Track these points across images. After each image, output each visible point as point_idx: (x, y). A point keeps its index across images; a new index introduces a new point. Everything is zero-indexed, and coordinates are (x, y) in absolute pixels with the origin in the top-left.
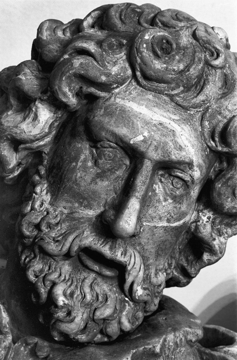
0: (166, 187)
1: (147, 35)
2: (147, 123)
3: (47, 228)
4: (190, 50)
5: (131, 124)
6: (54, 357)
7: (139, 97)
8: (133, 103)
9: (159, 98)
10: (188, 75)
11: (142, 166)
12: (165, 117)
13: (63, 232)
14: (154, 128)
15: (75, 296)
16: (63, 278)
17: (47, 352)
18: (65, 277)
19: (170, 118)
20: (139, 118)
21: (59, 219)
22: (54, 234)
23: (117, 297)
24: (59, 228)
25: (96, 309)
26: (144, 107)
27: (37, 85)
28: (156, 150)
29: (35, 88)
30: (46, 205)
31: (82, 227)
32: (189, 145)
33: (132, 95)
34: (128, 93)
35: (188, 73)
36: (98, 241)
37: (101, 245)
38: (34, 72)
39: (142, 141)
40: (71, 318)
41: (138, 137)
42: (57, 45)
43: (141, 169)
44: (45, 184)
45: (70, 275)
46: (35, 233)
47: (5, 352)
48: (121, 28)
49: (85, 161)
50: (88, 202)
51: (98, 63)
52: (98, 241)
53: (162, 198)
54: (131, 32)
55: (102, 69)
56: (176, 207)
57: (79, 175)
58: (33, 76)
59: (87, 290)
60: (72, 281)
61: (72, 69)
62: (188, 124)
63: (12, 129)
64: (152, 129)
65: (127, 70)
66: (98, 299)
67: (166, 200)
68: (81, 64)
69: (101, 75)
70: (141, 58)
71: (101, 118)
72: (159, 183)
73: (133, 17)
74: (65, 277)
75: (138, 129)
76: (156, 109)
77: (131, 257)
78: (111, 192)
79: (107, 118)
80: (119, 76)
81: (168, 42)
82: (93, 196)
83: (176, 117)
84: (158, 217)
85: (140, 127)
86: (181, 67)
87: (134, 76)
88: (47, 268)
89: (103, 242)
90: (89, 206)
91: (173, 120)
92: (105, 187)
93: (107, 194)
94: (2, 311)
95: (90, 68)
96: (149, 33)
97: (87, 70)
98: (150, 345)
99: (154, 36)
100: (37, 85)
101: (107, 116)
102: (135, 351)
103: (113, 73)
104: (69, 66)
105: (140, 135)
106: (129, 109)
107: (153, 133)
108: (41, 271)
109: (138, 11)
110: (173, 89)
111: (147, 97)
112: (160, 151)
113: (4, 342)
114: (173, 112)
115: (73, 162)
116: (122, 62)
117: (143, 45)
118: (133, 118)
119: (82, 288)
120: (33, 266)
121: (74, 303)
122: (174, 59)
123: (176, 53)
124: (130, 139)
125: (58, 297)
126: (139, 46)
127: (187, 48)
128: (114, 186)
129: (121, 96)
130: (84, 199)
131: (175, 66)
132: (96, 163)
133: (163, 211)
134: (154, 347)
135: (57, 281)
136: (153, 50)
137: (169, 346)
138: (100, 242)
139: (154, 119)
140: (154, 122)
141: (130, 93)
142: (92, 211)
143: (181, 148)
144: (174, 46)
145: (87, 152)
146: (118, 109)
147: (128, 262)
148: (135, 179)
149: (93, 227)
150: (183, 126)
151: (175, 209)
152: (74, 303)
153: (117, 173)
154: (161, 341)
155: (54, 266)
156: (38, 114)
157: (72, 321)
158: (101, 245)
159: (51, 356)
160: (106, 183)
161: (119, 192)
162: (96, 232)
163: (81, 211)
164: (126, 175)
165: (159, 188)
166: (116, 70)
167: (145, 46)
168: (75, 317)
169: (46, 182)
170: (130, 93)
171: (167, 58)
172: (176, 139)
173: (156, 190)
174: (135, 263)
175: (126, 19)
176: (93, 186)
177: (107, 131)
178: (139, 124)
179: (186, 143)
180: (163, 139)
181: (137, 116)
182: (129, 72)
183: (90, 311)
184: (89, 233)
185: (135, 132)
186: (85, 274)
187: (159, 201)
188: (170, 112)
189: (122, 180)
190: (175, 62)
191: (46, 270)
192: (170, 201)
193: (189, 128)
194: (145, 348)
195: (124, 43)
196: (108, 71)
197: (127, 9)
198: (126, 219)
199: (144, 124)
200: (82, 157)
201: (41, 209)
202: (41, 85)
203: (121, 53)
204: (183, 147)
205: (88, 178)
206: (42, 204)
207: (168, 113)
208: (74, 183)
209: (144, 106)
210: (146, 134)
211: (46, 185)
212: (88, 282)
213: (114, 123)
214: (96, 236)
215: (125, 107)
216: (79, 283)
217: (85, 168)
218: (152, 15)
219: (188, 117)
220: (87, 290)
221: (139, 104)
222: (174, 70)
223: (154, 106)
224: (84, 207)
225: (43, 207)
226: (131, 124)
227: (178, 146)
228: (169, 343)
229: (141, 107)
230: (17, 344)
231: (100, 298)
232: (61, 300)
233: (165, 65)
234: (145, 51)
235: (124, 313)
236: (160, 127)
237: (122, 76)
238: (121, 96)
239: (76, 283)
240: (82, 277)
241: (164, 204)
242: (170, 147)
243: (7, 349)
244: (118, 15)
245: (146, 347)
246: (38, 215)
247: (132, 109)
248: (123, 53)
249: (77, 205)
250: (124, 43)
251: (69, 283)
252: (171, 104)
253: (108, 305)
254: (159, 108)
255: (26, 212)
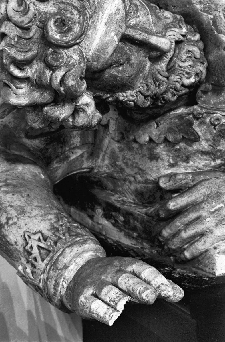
0: (133, 17)
1: (56, 37)
2: (106, 34)
3: (149, 91)
4: (61, 6)
5: (107, 44)
6: (214, 80)
7: (90, 39)
8: (93, 43)
9: (91, 26)
10: (80, 7)
11: (129, 35)
12: (101, 21)
13: (153, 81)
14: (109, 28)
15: (189, 71)
16: (179, 80)
17: (209, 85)
18: (179, 78)
19: (102, 18)
20: (103, 39)
21: (145, 85)
22: (153, 87)
23: (187, 45)
24: (150, 84)
25: (195, 58)
26: (96, 36)
27: (69, 106)
28: (121, 26)
29: (71, 107)
30: (133, 93)
31: (154, 70)
32: (114, 3)
33: (89, 44)
34: (86, 47)
35: (78, 7)
36: (164, 60)
37: (167, 58)
38: (59, 108)
39: (117, 36)
40: (200, 73)
41: (115, 40)
42: (35, 93)
43: (131, 36)
44: (119, 94)
45: (177, 75)
46: (149, 98)
47: (204, 109)
48: (35, 52)
49: (118, 71)
50: (142, 67)
51: (73, 69)
52: (164, 60)
53: (138, 19)
54: (39, 45)
55: (76, 66)
56: (141, 9)
57: (126, 75)
58: (62, 108)
59: (186, 64)
60: (181, 74)
61: (76, 85)
62: (103, 5)
63: (89, 119)
64: (110, 30)
65: (75, 49)
66: (190, 57)
67: (139, 17)
68: (73, 80)
69: (81, 67)
70: (72, 40)
71: (99, 64)
72: (130, 21)
73: (24, 43)
74: (179, 78)
75: (110, 40)
76: (97, 28)
77: (171, 38)
78: (139, 53)
79: (100, 60)
80: (80, 54)
81: (56, 22)
82: (140, 65)
83: (101, 13)
84: (148, 21)
85: (109, 38)
86: (76, 12)
87: (77, 44)
88: (171, 90)
89: (166, 57)
90: (144, 67)
91: (102, 15)
92: (135, 58)
93: (140, 56)
94: (176, 112)
95: (76, 74)
96: (54, 35)
97: (78, 76)
98: (210, 21)
99: (56, 32)
100: (69, 106)
101: (99, 60)
102: (215, 32)
103: (79, 58)
104: (72, 88)
105: (114, 38)
106: (97, 46)
107: (112, 30)
108: (172, 93)
109: (17, 39)
110: (87, 17)
111: (90, 35)
112: (121, 24)
113: (198, 110)
114: (98, 16)
115: (117, 79)
116: (69, 53)
117: (64, 40)
118: (103, 43)
119: (185, 68)
120: (169, 98)
121: (193, 72)
122: (71, 18)
123: (64, 16)
124: (116, 44)
125: (191, 82)
126: (64, 42)
127: (59, 8)
128: (135, 52)
129: (88, 51)
130: (140, 70)
131: (77, 17)
132: (122, 65)
133: (145, 18)
134: (211, 19)
135: (181, 83)
136: (67, 32)
137: (203, 8)
138: (165, 58)
139: (103, 29)
140: (105, 28)
141: (87, 45)
142: (147, 65)
143: (118, 10)
144: (58, 17)
145: (113, 70)
146: (96, 53)
147: (175, 40)
148: (137, 40)
149: (155, 63)
150: (105, 8)
151: (142, 9)
152: (193, 72)
153: (126, 50)
154: (205, 14)
155: (172, 86)
156: (86, 103)
157: (202, 72)
158: (167, 58)
159: (212, 82)
160: (133, 57)
161: (140, 49)
162: (158, 61)
163: (146, 72)
164: (129, 44)
165: (132, 22)
166: (76, 56)
167: (65, 38)
168: (200, 70)
169: (117, 94)
170: (87, 45)
171: (70, 23)
172: (113, 13)
173: (134, 24)
174: (174, 35)
175: (26, 48)
176: (134, 66)
177: (109, 59)
178: (107, 39)
179: (114, 6)
180: (114, 22)
181: (102, 41)
182: (76, 47)
183: (196, 61)
184: (158, 66)
185: (112, 41)
186: (177, 66)
187: (140, 21)
188: (98, 18)
189: (132, 47)
190: (73, 17)
191: (172, 90)
192: (139, 13)
193: (105, 4)
194: (212, 25)
195: (52, 50)
196: (77, 62)
197: (17, 47)
198: (164, 45)
199: (107, 35)
200: (116, 73)
201: (135, 96)
202: (69, 103)
203: (62, 53)
204: (116, 8)
205: (130, 69)
206: (133, 96)
207: (99, 19)
208: (130, 78)
209: (96, 36)
210: (113, 34)
211: (120, 94)
212: (181, 64)
213: (105, 55)
214: (161, 61)
215: (95, 49)
216: (182, 69)
217: (123, 71)
218: (17, 28)
219: (99, 5)
220: (186, 64)
221: (94, 40)
222: (79, 18)
223: (96, 29)
224: (144, 70)
225: (134, 95)
226: (107, 44)
227: (117, 12)
228: (202, 8)
229: (96, 38)
230: (199, 103)
231: (190, 55)
232: (192, 80)
233: (77, 24)
234: (69, 38)
235: (192, 39)
236: (107, 25)
237: (79, 52)
238: (88, 51)
239: (182, 72)
240: (178, 68)
241: (141, 18)
242: (119, 17)
243: (202, 108)
244: (23, 54)
245: (211, 24)
246: (140, 98)
247: (97, 44)
248: (63, 52)
249: (141, 74)
250: (52, 50)
251: (182, 76)
252: (94, 18)
253: (193, 50)
254: (97, 26)
255: (134, 105)
